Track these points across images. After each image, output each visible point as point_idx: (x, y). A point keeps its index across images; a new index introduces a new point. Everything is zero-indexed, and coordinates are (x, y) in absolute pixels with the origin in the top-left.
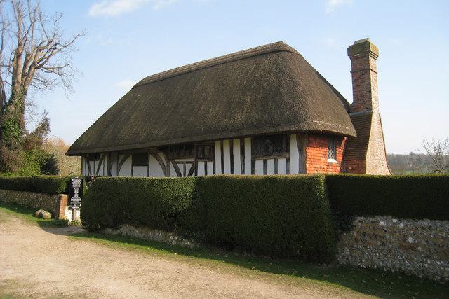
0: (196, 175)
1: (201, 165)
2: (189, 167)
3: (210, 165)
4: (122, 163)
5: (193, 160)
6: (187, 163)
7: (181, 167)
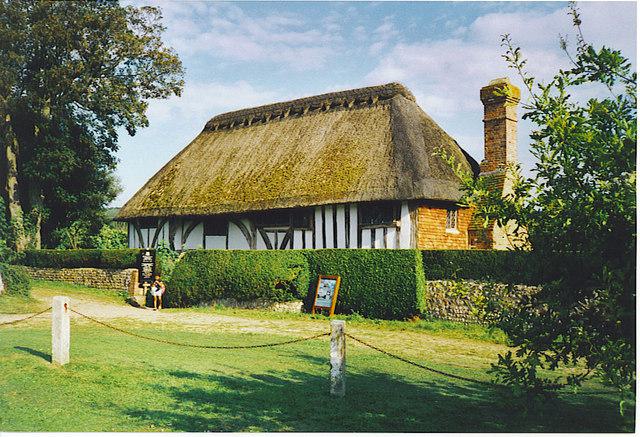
0: (292, 247)
1: (298, 235)
2: (281, 236)
3: (309, 235)
4: (188, 232)
5: (287, 228)
6: (280, 231)
7: (271, 236)
